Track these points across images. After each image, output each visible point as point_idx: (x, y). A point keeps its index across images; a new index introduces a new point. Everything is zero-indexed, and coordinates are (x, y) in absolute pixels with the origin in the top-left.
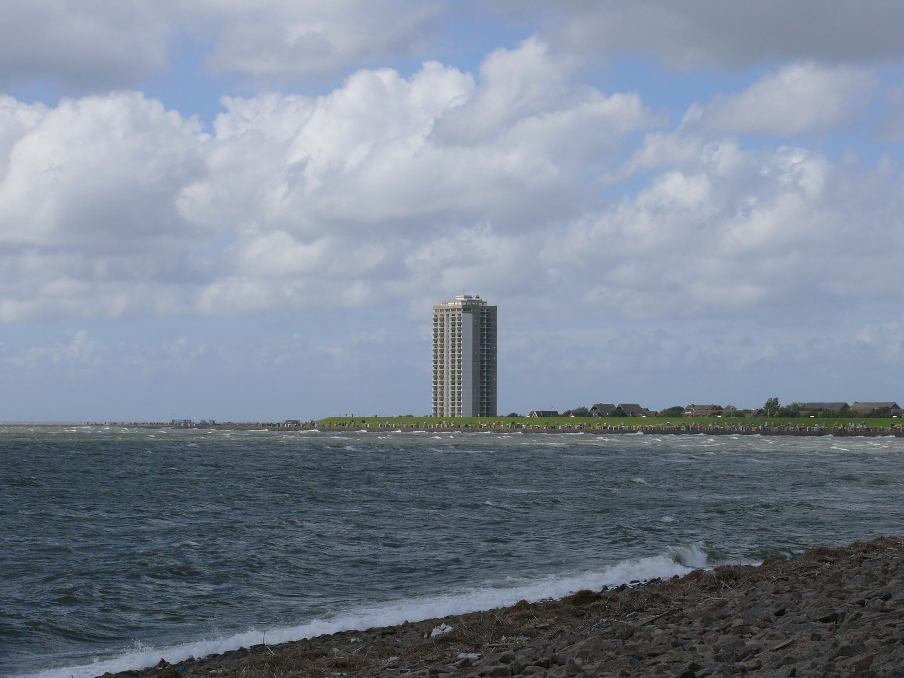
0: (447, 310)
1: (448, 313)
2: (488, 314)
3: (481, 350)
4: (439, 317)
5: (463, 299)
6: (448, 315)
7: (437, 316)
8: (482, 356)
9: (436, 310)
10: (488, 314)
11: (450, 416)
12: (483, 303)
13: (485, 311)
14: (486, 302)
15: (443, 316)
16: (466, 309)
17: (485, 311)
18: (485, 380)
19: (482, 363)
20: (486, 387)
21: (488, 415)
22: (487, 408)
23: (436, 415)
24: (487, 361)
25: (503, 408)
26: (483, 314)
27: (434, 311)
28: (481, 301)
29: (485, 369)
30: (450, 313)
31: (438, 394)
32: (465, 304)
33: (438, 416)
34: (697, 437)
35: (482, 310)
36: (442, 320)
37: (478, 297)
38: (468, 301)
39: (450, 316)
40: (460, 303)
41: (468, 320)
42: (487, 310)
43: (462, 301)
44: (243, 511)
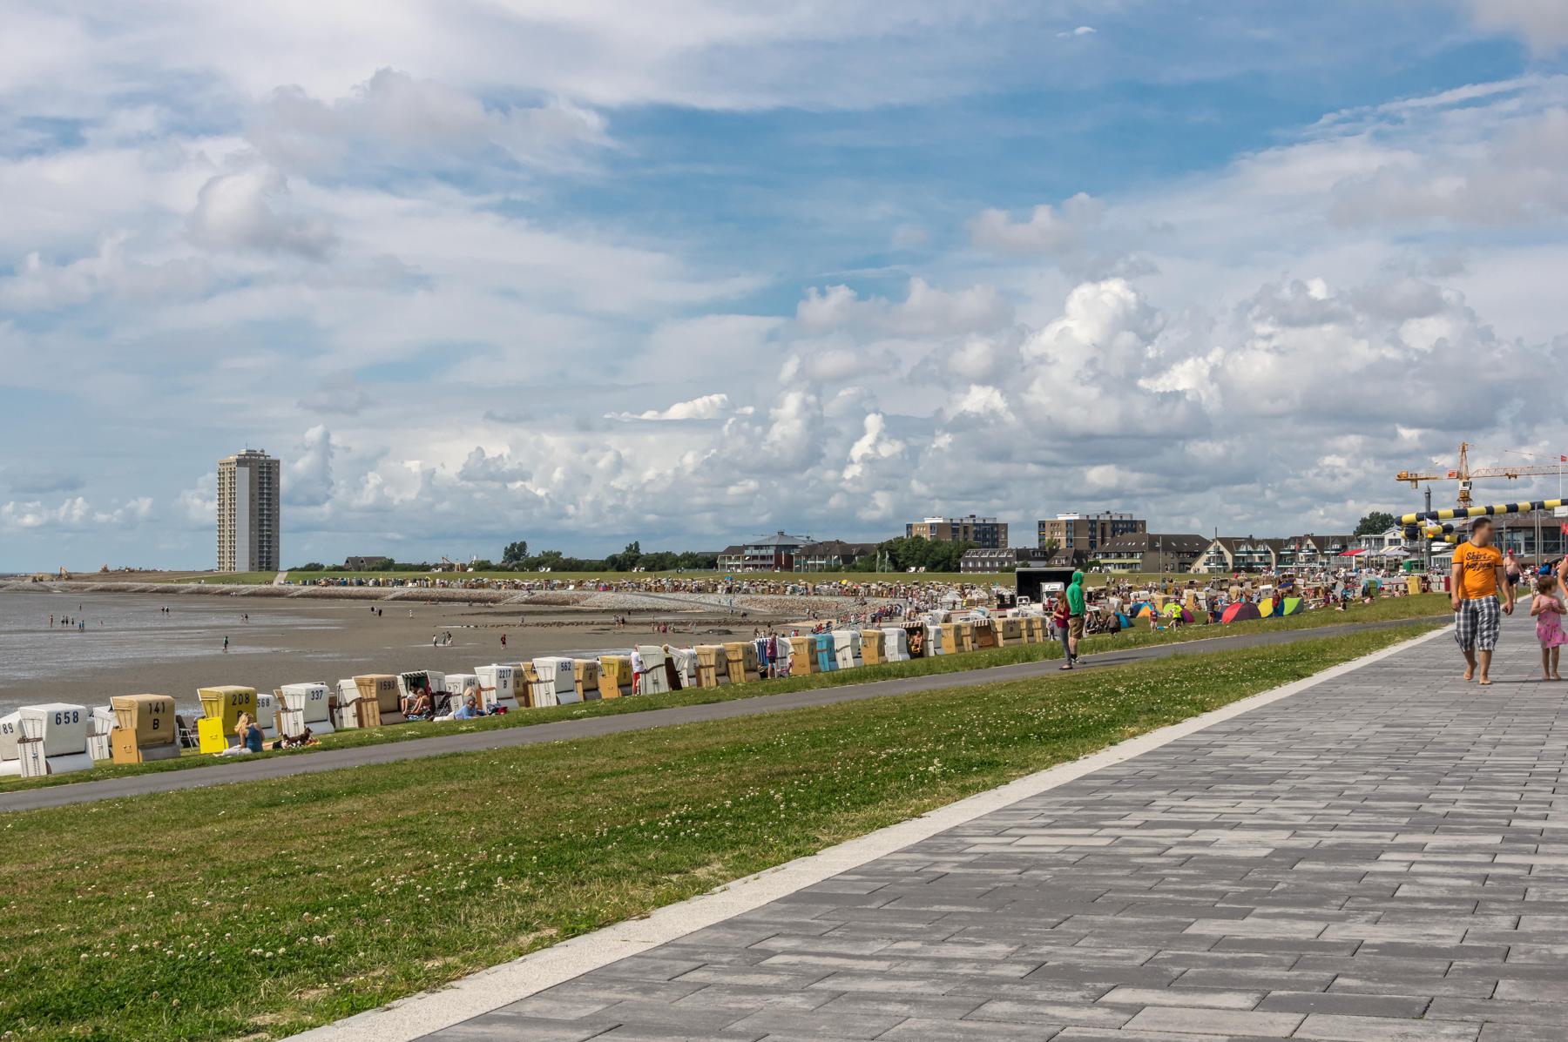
10: (269, 468)
37: (263, 451)
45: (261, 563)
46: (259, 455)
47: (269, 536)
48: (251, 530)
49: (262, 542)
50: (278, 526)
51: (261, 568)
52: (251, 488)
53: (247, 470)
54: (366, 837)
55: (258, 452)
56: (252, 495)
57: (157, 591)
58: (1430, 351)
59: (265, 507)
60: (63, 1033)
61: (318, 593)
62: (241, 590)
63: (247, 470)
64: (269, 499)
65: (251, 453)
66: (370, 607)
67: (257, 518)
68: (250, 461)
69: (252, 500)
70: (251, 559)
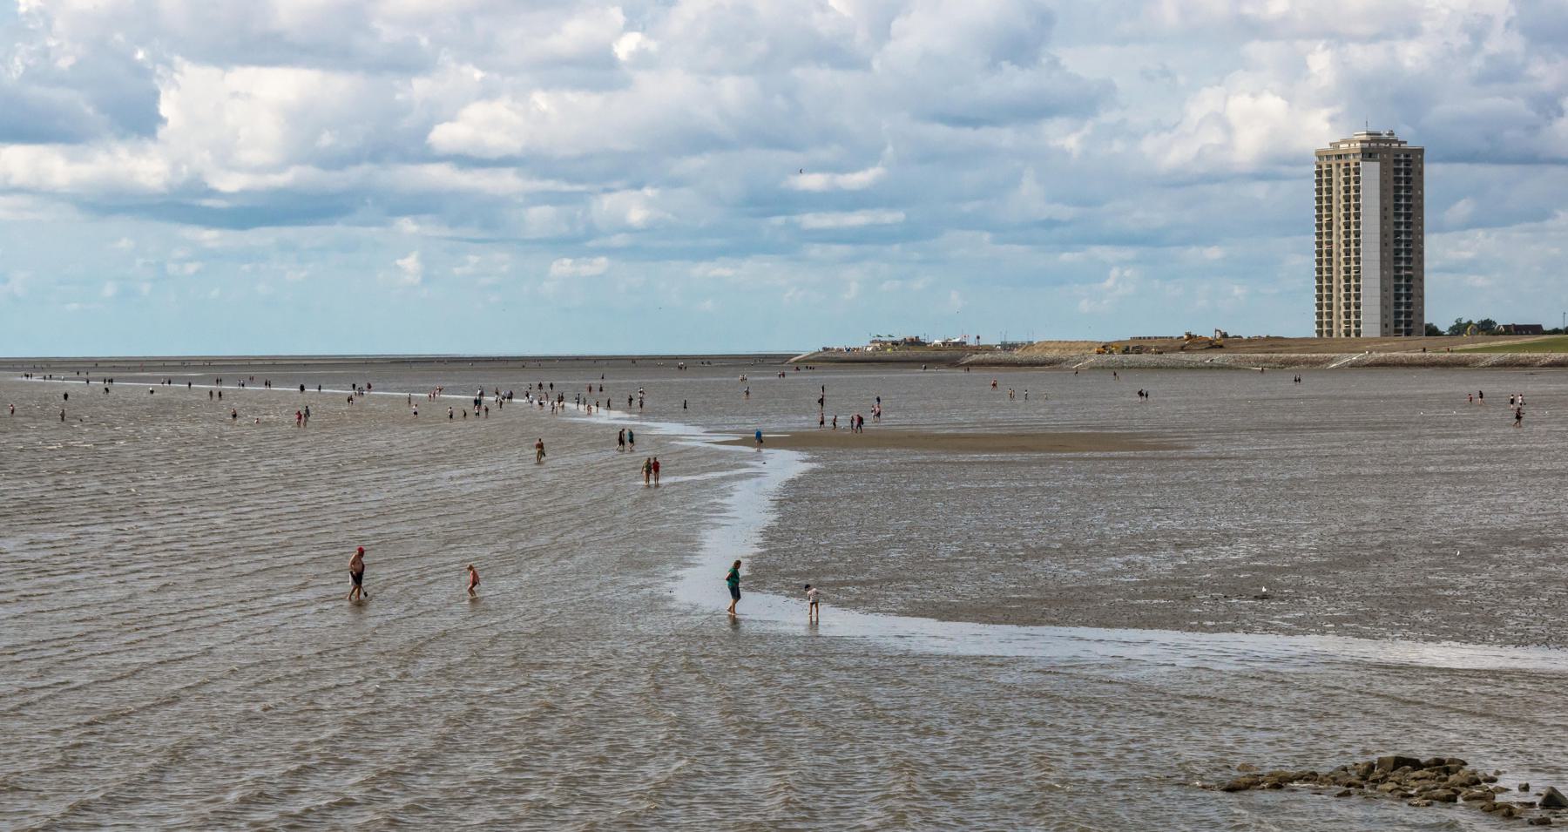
0: (1339, 157)
1: (1339, 161)
2: (1408, 162)
3: (1395, 169)
4: (1324, 168)
5: (1364, 137)
6: (1339, 165)
7: (1321, 167)
8: (1398, 234)
9: (1320, 157)
10: (1408, 162)
11: (1343, 336)
12: (1400, 143)
13: (1402, 157)
14: (1405, 142)
15: (1331, 166)
16: (1368, 154)
17: (1402, 157)
18: (1403, 211)
19: (1398, 299)
20: (1405, 232)
21: (1408, 333)
22: (1406, 214)
23: (1320, 333)
24: (1405, 232)
25: (1439, 310)
26: (1398, 162)
27: (1316, 159)
28: (1396, 141)
29: (1403, 300)
30: (1342, 162)
31: (1324, 281)
32: (1367, 145)
33: (1325, 335)
34: (1371, 473)
35: (1398, 156)
36: (1329, 173)
37: (1391, 134)
38: (1372, 141)
39: (1343, 167)
40: (1358, 145)
41: (1371, 173)
42: (1407, 156)
43: (1362, 142)
44: (489, 531)
45: (1397, 323)
46: (1386, 141)
47: (1408, 278)
48: (1382, 268)
49: (1397, 288)
50: (1421, 261)
51: (1398, 332)
52: (1382, 198)
53: (1376, 165)
54: (407, 589)
55: (1385, 136)
56: (1384, 209)
57: (1370, 365)
58: (428, 142)
59: (1403, 228)
60: (667, 765)
61: (1417, 361)
62: (1540, 359)
63: (1376, 165)
64: (1408, 216)
65: (1375, 137)
66: (155, 394)
67: (1393, 247)
68: (1381, 151)
69: (1384, 218)
70: (1384, 316)
